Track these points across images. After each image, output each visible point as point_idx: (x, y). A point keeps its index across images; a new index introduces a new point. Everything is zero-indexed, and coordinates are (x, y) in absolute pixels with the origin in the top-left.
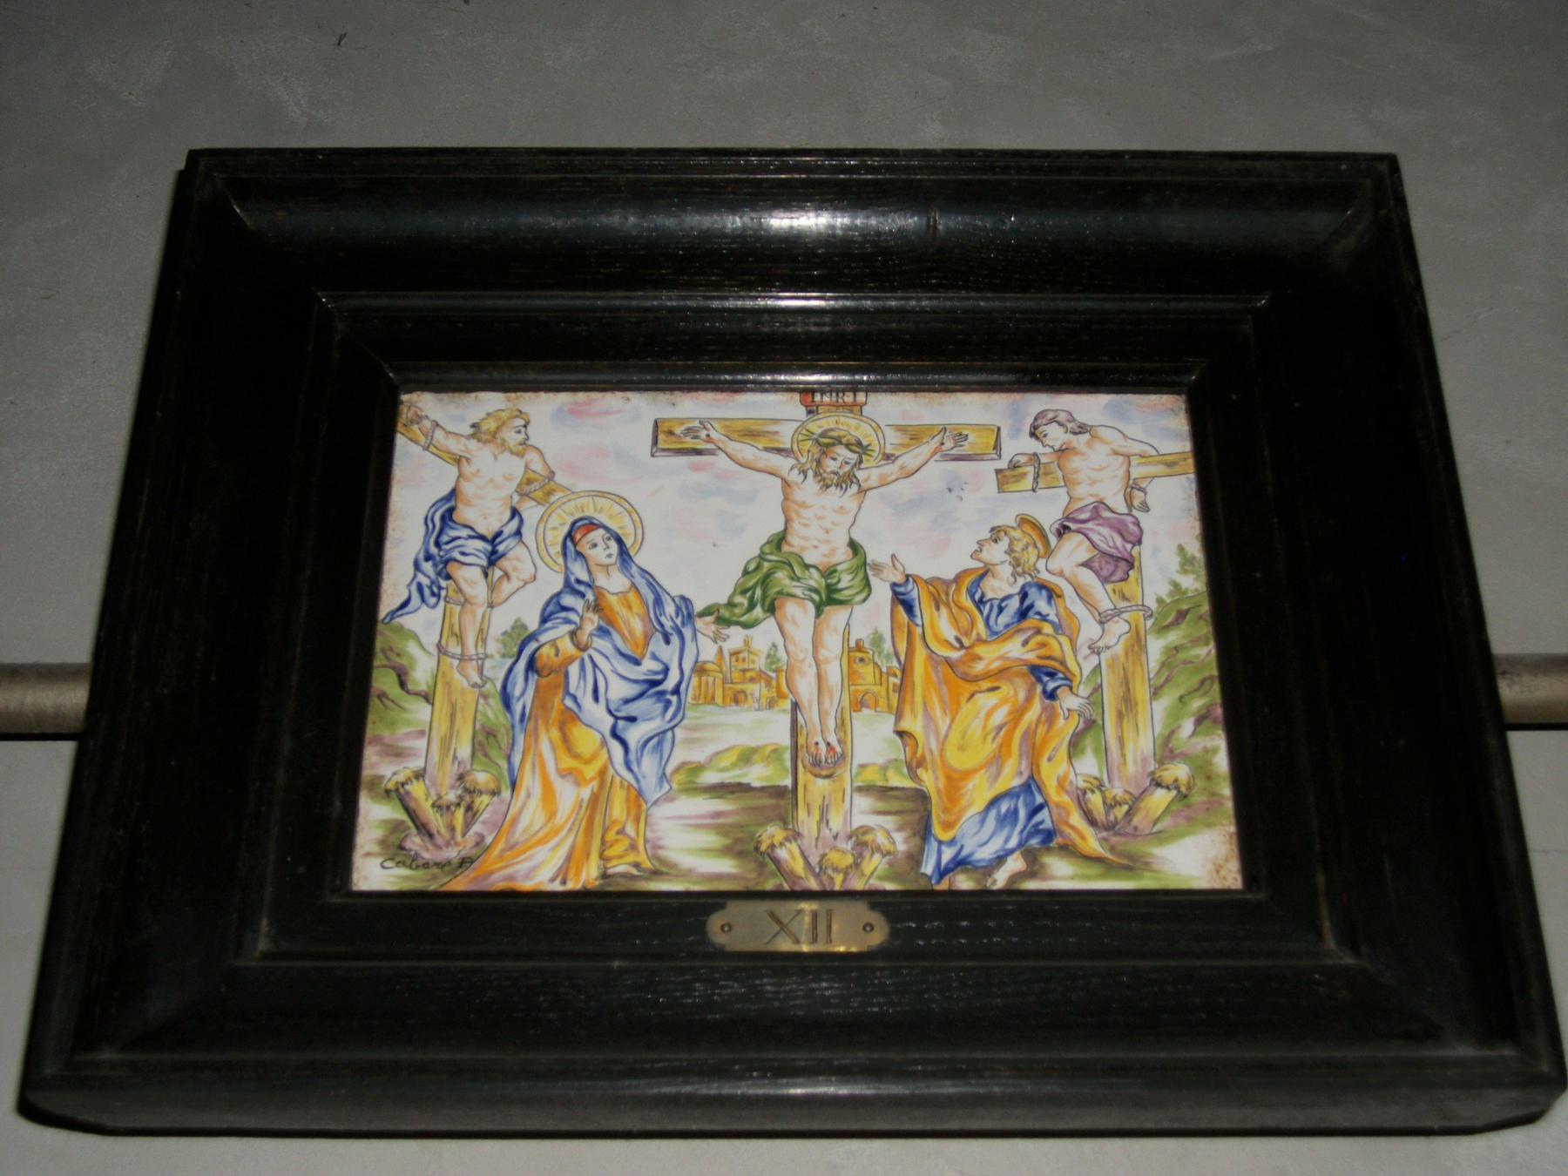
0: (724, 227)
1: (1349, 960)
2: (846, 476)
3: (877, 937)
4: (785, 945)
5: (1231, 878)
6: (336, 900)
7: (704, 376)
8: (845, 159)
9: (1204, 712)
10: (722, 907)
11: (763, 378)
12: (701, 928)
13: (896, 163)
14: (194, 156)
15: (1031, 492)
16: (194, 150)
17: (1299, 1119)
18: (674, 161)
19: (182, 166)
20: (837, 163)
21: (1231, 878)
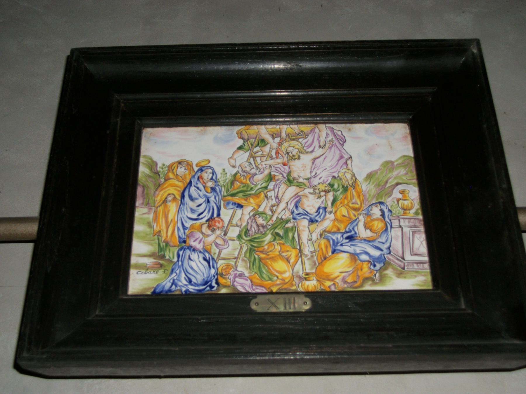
0: (259, 68)
1: (470, 311)
2: (299, 152)
3: (307, 307)
4: (273, 310)
5: (429, 286)
6: (125, 297)
7: (262, 120)
8: (265, 46)
9: (180, 277)
10: (255, 297)
11: (277, 120)
12: (249, 304)
13: (228, 48)
14: (73, 51)
15: (239, 172)
16: (77, 49)
17: (441, 368)
18: (305, 46)
19: (69, 54)
20: (287, 47)
21: (429, 286)
